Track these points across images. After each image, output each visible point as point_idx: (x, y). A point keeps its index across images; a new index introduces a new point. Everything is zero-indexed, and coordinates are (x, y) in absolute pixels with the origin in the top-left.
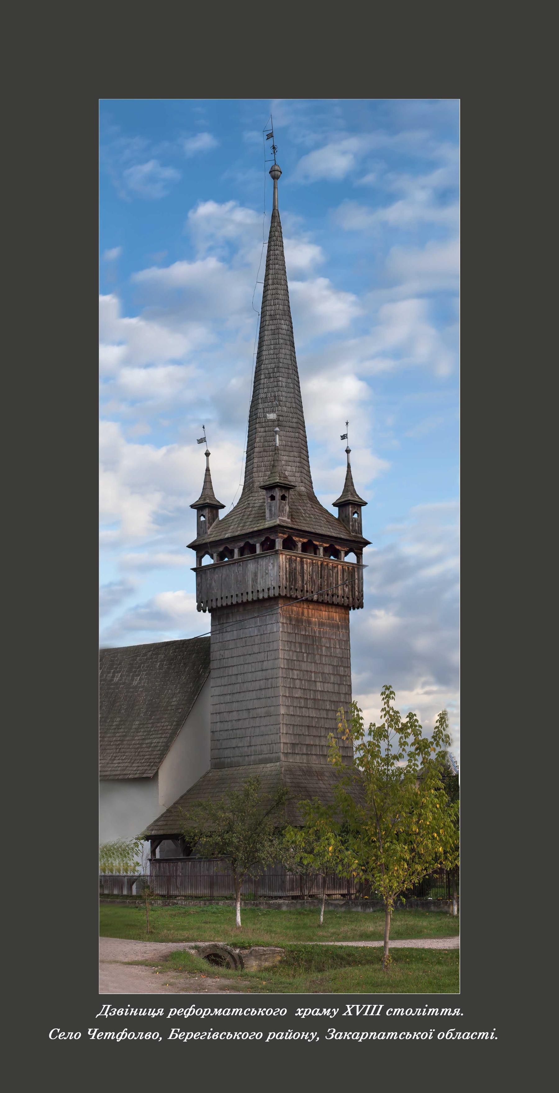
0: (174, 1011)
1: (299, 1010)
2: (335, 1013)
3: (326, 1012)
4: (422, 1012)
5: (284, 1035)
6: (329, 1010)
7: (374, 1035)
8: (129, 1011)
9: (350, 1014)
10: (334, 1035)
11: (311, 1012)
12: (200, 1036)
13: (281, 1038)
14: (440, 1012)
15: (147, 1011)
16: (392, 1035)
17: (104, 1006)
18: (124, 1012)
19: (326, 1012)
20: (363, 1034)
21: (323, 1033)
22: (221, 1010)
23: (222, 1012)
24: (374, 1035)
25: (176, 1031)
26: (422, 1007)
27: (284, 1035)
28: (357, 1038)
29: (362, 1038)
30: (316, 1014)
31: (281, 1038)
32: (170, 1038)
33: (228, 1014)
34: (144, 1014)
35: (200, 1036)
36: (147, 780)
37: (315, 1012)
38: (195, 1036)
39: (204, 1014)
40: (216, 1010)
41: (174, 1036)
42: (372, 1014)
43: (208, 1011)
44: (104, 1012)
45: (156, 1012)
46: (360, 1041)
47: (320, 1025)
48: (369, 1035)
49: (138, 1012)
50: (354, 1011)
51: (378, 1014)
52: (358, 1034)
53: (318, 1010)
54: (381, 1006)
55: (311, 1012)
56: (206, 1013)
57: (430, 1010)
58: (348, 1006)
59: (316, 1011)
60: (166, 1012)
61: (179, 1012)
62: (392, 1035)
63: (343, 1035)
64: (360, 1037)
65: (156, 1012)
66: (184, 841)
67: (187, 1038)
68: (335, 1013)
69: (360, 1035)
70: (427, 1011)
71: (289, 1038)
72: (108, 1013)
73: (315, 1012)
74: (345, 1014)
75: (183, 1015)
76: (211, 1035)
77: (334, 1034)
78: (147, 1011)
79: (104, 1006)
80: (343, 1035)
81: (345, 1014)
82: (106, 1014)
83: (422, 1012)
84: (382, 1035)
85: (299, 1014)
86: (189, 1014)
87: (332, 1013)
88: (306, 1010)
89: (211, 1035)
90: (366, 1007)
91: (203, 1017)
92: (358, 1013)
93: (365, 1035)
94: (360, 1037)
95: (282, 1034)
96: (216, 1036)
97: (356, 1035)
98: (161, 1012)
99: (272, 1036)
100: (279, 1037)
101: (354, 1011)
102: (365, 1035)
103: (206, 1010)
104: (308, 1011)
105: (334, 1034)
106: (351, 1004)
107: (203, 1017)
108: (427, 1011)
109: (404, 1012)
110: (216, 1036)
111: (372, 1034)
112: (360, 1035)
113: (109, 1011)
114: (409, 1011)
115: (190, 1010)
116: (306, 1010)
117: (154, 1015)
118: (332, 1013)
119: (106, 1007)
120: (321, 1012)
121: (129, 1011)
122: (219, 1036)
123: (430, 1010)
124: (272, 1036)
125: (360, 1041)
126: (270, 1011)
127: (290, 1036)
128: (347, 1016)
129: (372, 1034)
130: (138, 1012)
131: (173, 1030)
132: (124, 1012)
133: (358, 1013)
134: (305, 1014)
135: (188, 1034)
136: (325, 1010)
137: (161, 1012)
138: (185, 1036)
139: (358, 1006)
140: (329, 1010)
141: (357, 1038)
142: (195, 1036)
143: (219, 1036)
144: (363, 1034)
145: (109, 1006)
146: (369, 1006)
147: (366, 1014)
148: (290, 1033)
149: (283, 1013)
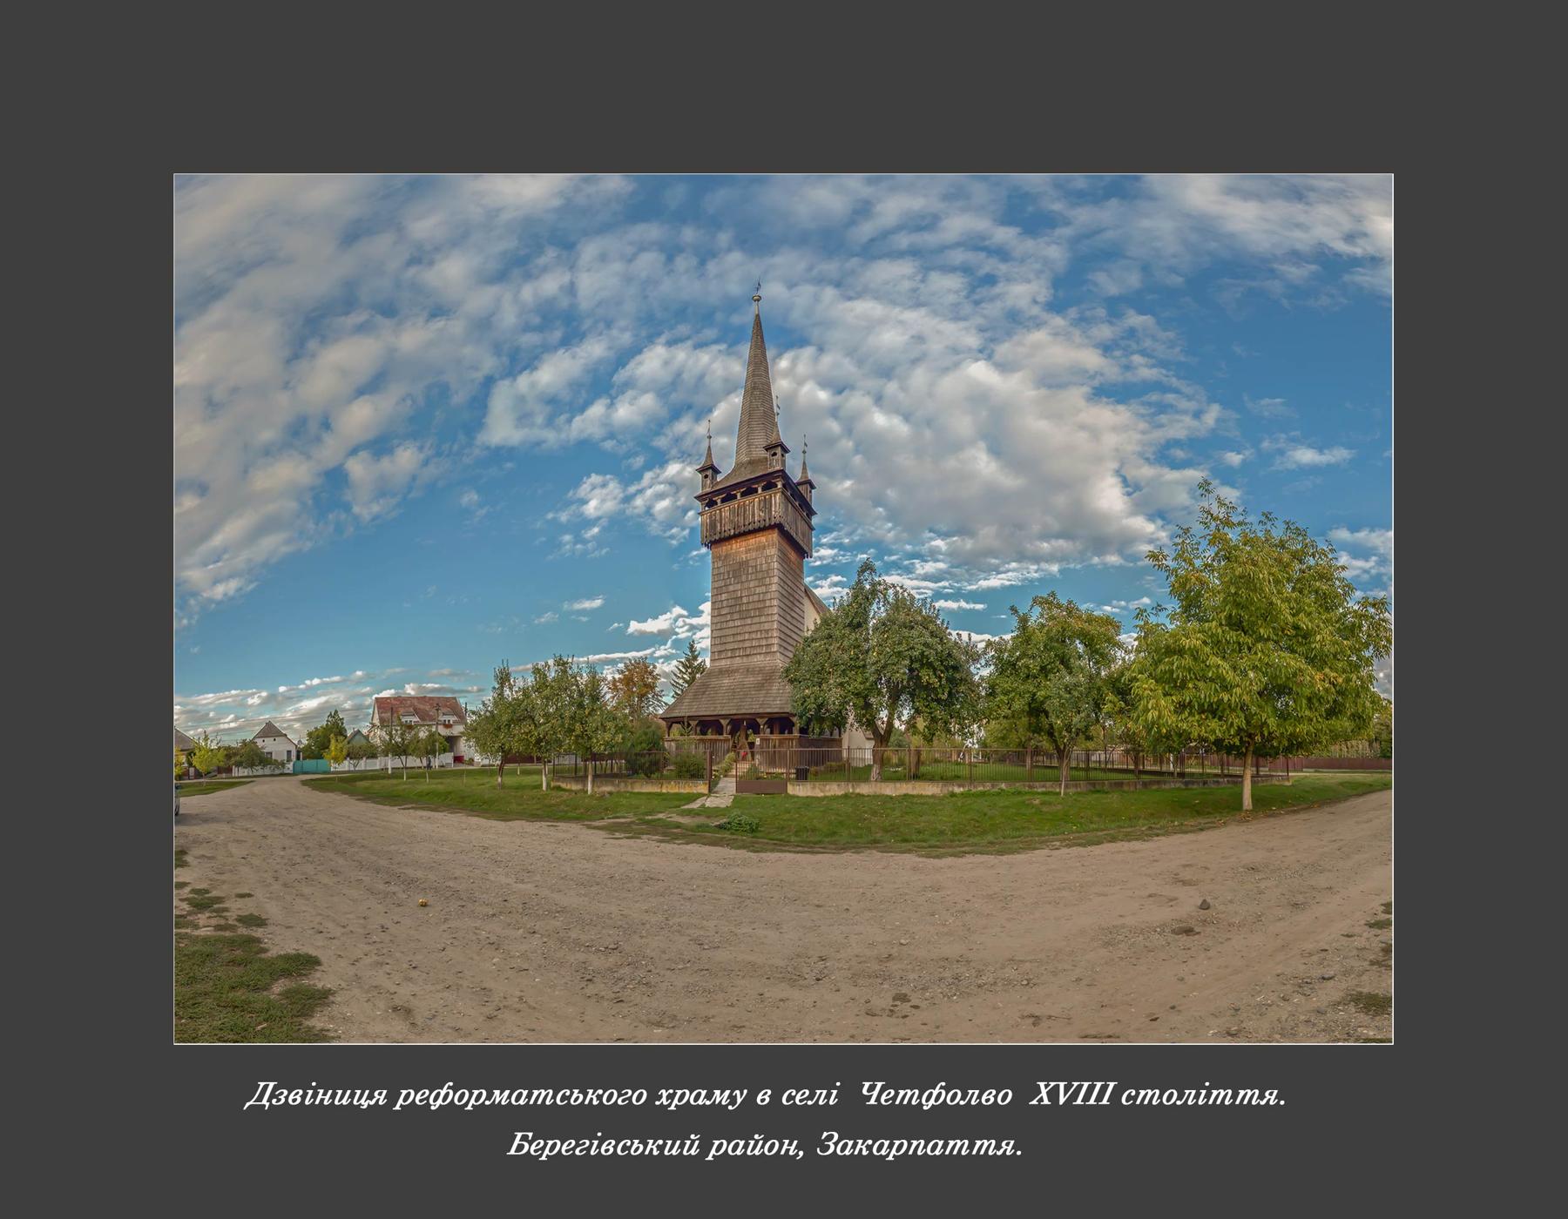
0: (408, 1095)
1: (664, 1093)
2: (739, 1100)
3: (721, 1097)
4: (1197, 1096)
5: (746, 1146)
6: (727, 1092)
7: (919, 1147)
8: (315, 1096)
9: (1046, 1102)
10: (836, 1145)
11: (689, 1097)
12: (574, 1149)
13: (738, 1152)
14: (1234, 1097)
15: (352, 1096)
16: (959, 1146)
17: (262, 1084)
18: (304, 1097)
19: (721, 1097)
20: (897, 1143)
21: (810, 1142)
22: (507, 1092)
23: (509, 1097)
24: (919, 1147)
25: (524, 1138)
26: (1198, 1089)
27: (746, 1146)
28: (883, 1152)
29: (894, 1152)
30: (700, 1102)
31: (738, 1152)
32: (512, 1152)
33: (522, 1102)
34: (344, 1102)
35: (574, 1149)
36: (1321, 451)
37: (696, 1099)
38: (564, 1148)
39: (472, 1101)
40: (497, 1092)
41: (520, 1147)
42: (1092, 1102)
43: (480, 1095)
44: (260, 1098)
45: (370, 1097)
46: (890, 1158)
47: (806, 1124)
48: (910, 1145)
49: (333, 1097)
50: (1053, 1094)
51: (1105, 1102)
52: (887, 1143)
53: (704, 1093)
54: (1112, 1085)
55: (689, 1097)
56: (477, 1099)
57: (1215, 1093)
58: (1042, 1085)
59: (699, 1095)
60: (392, 1098)
61: (418, 1097)
62: (959, 1146)
63: (854, 1146)
64: (889, 1150)
65: (370, 1097)
66: (788, 484)
67: (547, 1152)
68: (739, 1100)
69: (891, 1146)
70: (1208, 1096)
71: (756, 1152)
72: (269, 1100)
73: (696, 1099)
74: (1034, 1102)
75: (428, 1105)
76: (599, 1147)
77: (836, 1144)
78: (352, 1096)
79: (262, 1084)
80: (854, 1146)
81: (1034, 1102)
82: (265, 1102)
83: (1197, 1096)
84: (935, 1146)
85: (664, 1101)
86: (440, 1102)
87: (732, 1099)
88: (679, 1092)
89: (599, 1147)
90: (1080, 1087)
91: (469, 1108)
92: (1062, 1100)
93: (901, 1145)
94: (889, 1150)
95: (742, 1143)
96: (608, 1148)
97: (881, 1146)
98: (380, 1097)
99: (722, 1147)
100: (734, 1150)
101: (1053, 1094)
102: (901, 1145)
103: (476, 1092)
104: (683, 1095)
105: (836, 1144)
106: (1048, 1080)
107: (469, 1108)
108: (1208, 1096)
109: (1160, 1097)
110: (608, 1148)
111: (915, 1143)
112: (891, 1146)
113: (272, 1096)
114: (1171, 1095)
115: (443, 1093)
116: (679, 1092)
117: (365, 1104)
118: (732, 1099)
119: (266, 1087)
120: (708, 1097)
121: (315, 1096)
122: (615, 1147)
123: (1215, 1093)
124: (722, 1147)
125: (890, 1158)
126: (611, 1095)
127: (759, 1147)
128: (1040, 1106)
129: (915, 1143)
130: (333, 1097)
131: (519, 1135)
132: (304, 1097)
133: (1062, 1100)
134: (676, 1101)
135: (550, 1143)
136: (717, 1092)
137: (380, 1097)
138: (543, 1149)
139: (1062, 1085)
140: (727, 1092)
141: (883, 1152)
142: (564, 1148)
143: (615, 1147)
144: (897, 1143)
145: (272, 1085)
146: (1086, 1085)
147: (1079, 1102)
148: (757, 1142)
149: (638, 1099)
